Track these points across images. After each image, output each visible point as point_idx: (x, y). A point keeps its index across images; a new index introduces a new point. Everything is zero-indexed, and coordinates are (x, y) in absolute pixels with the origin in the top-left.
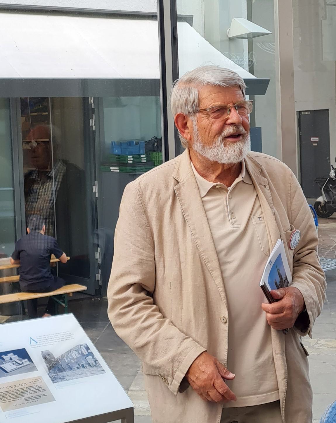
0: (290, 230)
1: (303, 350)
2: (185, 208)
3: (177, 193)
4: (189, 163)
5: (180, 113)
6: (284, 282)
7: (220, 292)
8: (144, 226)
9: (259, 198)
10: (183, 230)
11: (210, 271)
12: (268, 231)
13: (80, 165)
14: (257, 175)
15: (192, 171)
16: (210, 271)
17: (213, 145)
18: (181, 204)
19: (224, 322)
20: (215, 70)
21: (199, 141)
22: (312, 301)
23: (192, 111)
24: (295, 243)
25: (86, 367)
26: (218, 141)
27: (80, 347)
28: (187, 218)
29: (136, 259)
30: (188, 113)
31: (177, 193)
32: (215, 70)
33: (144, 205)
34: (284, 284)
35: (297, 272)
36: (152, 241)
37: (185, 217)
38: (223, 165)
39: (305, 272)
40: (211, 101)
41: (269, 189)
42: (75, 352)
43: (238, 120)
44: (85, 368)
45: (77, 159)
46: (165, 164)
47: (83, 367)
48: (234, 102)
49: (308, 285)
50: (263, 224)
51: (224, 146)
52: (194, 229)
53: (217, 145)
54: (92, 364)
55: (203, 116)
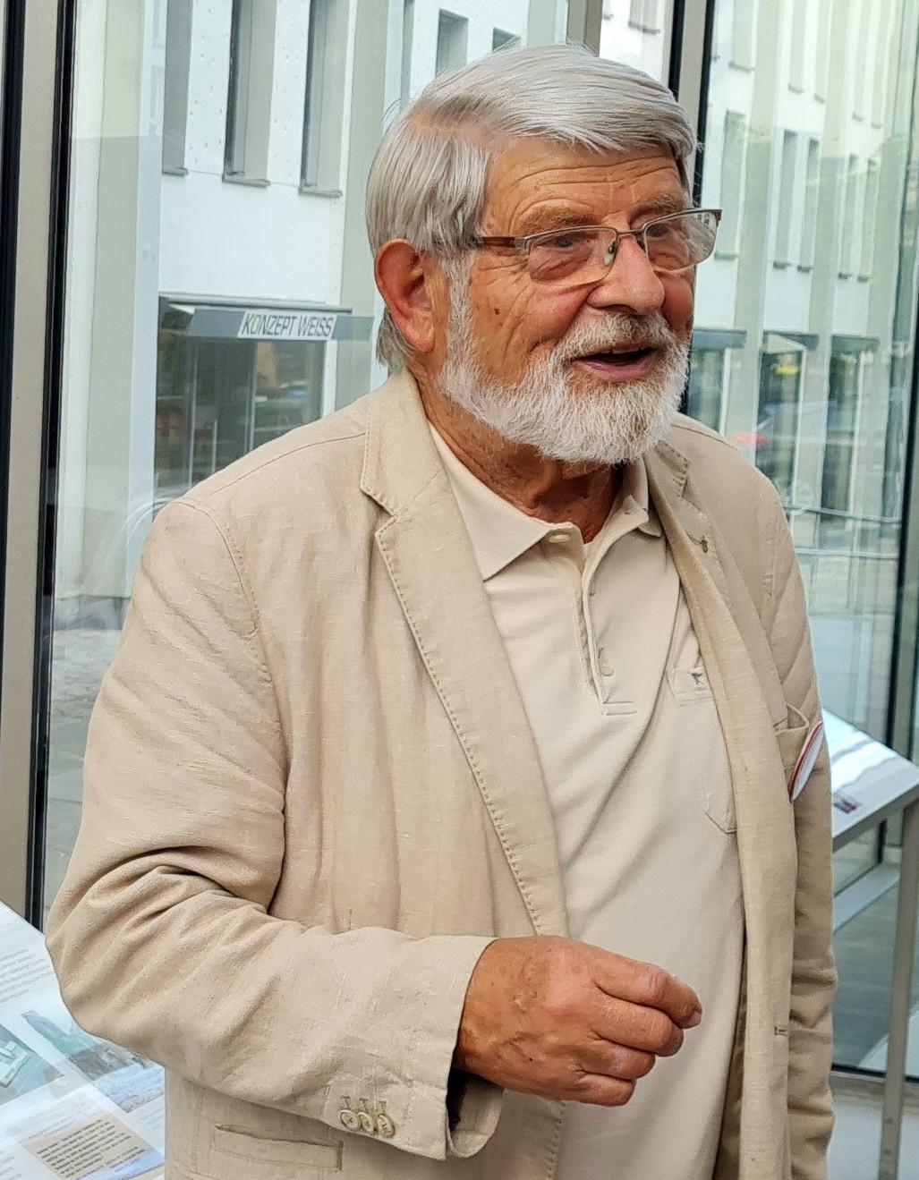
5: (399, 240)
21: (465, 359)
23: (450, 240)
26: (546, 364)
30: (434, 242)
38: (560, 464)
53: (537, 383)
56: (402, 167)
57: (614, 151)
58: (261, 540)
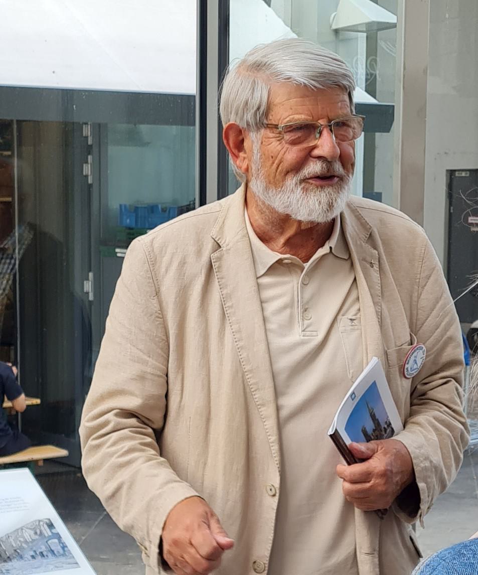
0: (406, 344)
1: (412, 549)
2: (227, 294)
3: (215, 266)
4: (242, 213)
5: (233, 122)
6: (383, 429)
7: (271, 443)
8: (153, 317)
9: (358, 285)
10: (219, 331)
11: (258, 405)
12: (364, 343)
13: (58, 235)
14: (361, 243)
15: (245, 228)
16: (258, 405)
17: (283, 189)
18: (220, 285)
19: (272, 494)
20: (303, 52)
21: (260, 177)
22: (427, 464)
24: (415, 366)
25: (47, 556)
26: (291, 181)
27: (39, 523)
28: (228, 312)
29: (135, 369)
31: (215, 266)
32: (303, 52)
33: (157, 280)
34: (383, 433)
35: (415, 415)
36: (166, 346)
37: (225, 309)
38: (300, 222)
39: (425, 417)
40: (288, 112)
41: (378, 269)
42: (30, 531)
43: (332, 153)
44: (46, 557)
45: (53, 227)
46: (200, 210)
47: (41, 557)
48: (331, 115)
49: (425, 437)
50: (358, 332)
51: (302, 192)
52: (239, 331)
54: (58, 552)
55: (271, 135)
56: (235, 90)
57: (321, 89)
58: (164, 257)
